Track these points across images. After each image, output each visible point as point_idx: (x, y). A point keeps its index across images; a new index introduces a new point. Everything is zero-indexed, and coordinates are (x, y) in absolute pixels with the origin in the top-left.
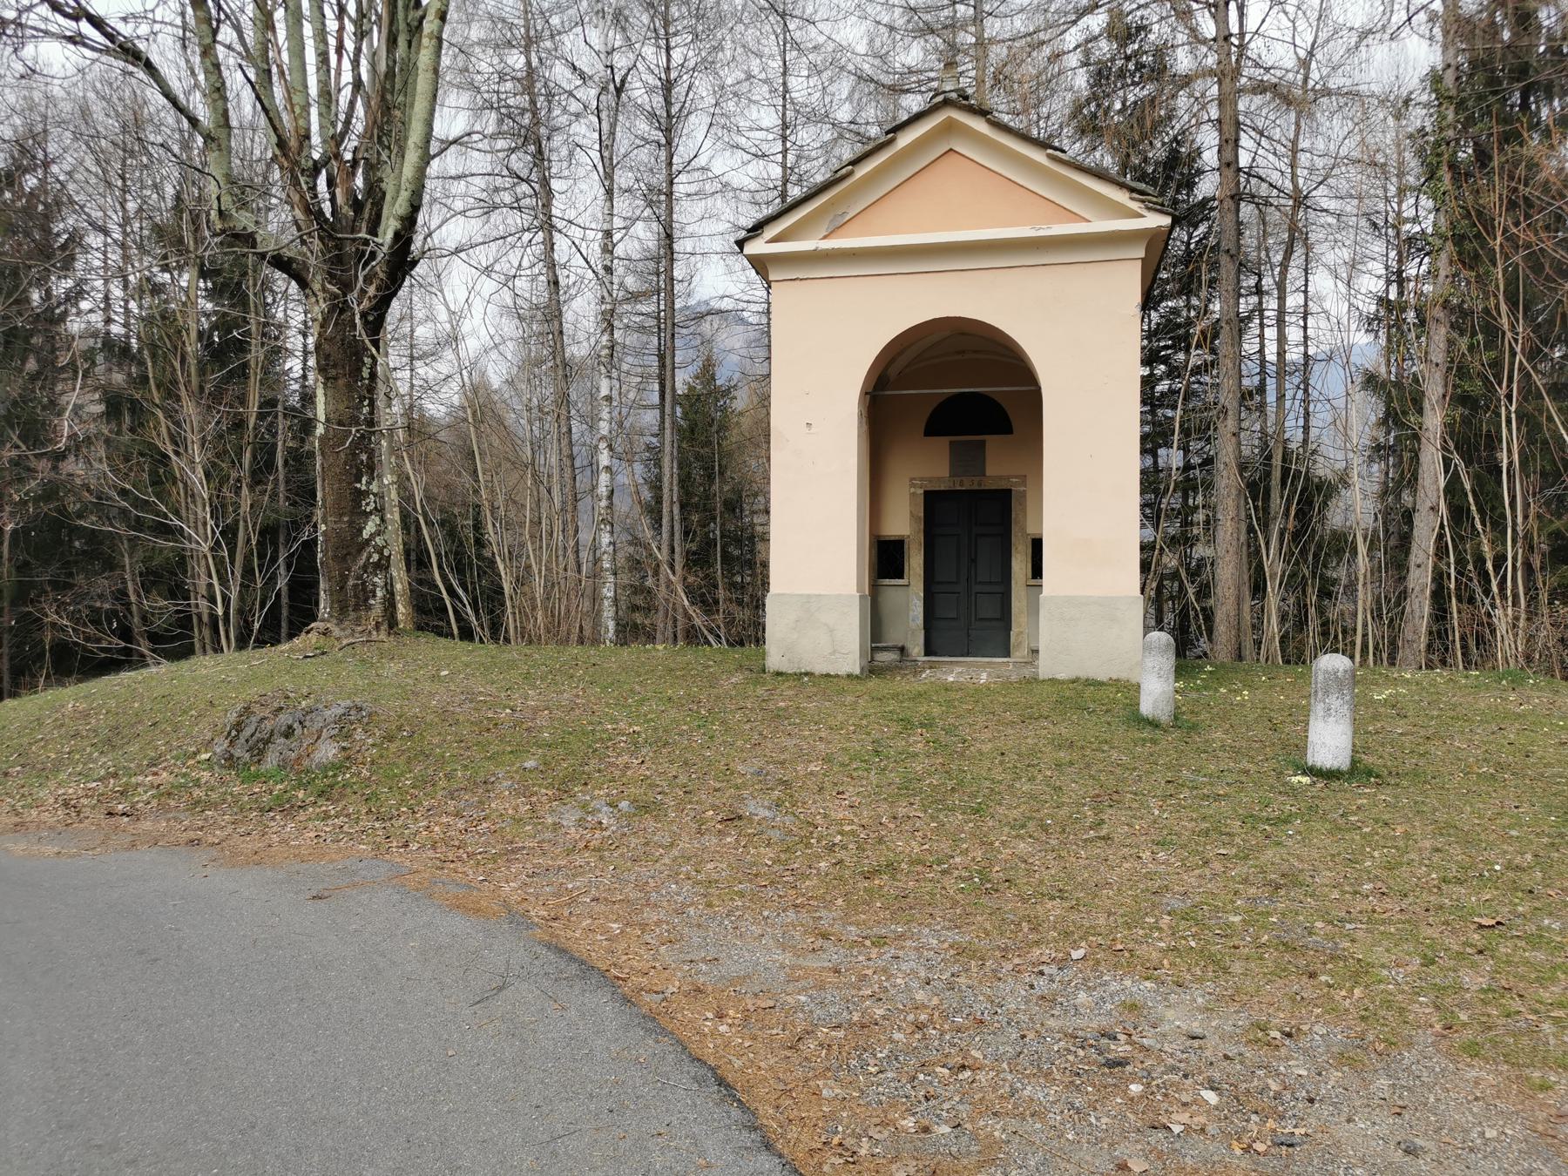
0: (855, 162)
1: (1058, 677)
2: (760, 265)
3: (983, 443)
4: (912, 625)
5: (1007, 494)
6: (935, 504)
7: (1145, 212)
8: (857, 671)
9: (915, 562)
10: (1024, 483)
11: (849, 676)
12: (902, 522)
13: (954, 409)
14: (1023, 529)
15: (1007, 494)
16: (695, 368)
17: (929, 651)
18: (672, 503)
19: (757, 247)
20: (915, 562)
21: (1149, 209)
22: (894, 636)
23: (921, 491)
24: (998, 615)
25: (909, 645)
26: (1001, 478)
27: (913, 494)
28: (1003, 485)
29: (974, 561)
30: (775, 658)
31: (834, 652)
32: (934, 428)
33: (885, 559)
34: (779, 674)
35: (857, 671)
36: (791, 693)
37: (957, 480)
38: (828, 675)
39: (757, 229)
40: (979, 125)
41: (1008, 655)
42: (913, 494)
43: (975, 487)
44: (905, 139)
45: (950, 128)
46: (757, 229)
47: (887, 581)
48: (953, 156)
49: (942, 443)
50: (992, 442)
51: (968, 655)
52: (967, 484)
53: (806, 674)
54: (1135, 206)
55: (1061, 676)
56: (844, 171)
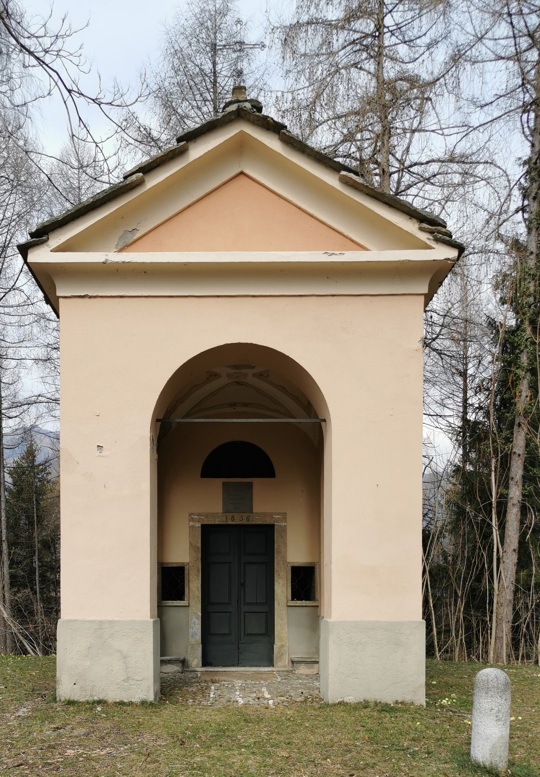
0: (147, 169)
1: (347, 700)
2: (46, 279)
3: (250, 486)
4: (192, 640)
5: (271, 527)
6: (211, 536)
7: (433, 244)
8: (151, 698)
9: (194, 586)
10: (285, 519)
11: (143, 703)
12: (183, 552)
13: (239, 441)
14: (284, 558)
15: (271, 527)
16: (21, 451)
17: (206, 662)
18: (491, 629)
19: (41, 255)
20: (194, 586)
21: (437, 240)
22: (177, 651)
23: (198, 525)
24: (263, 631)
25: (189, 658)
26: (264, 514)
27: (192, 527)
28: (268, 521)
29: (243, 585)
30: (66, 689)
31: (127, 679)
32: (210, 471)
33: (169, 583)
34: (70, 703)
35: (151, 698)
36: (81, 731)
37: (230, 515)
38: (121, 703)
39: (41, 235)
40: (273, 143)
41: (271, 663)
42: (192, 527)
43: (245, 522)
44: (198, 151)
45: (241, 147)
46: (41, 235)
47: (170, 603)
48: (243, 180)
49: (217, 483)
50: (258, 483)
51: (238, 665)
52: (238, 519)
53: (99, 702)
54: (424, 237)
55: (350, 699)
56: (134, 177)
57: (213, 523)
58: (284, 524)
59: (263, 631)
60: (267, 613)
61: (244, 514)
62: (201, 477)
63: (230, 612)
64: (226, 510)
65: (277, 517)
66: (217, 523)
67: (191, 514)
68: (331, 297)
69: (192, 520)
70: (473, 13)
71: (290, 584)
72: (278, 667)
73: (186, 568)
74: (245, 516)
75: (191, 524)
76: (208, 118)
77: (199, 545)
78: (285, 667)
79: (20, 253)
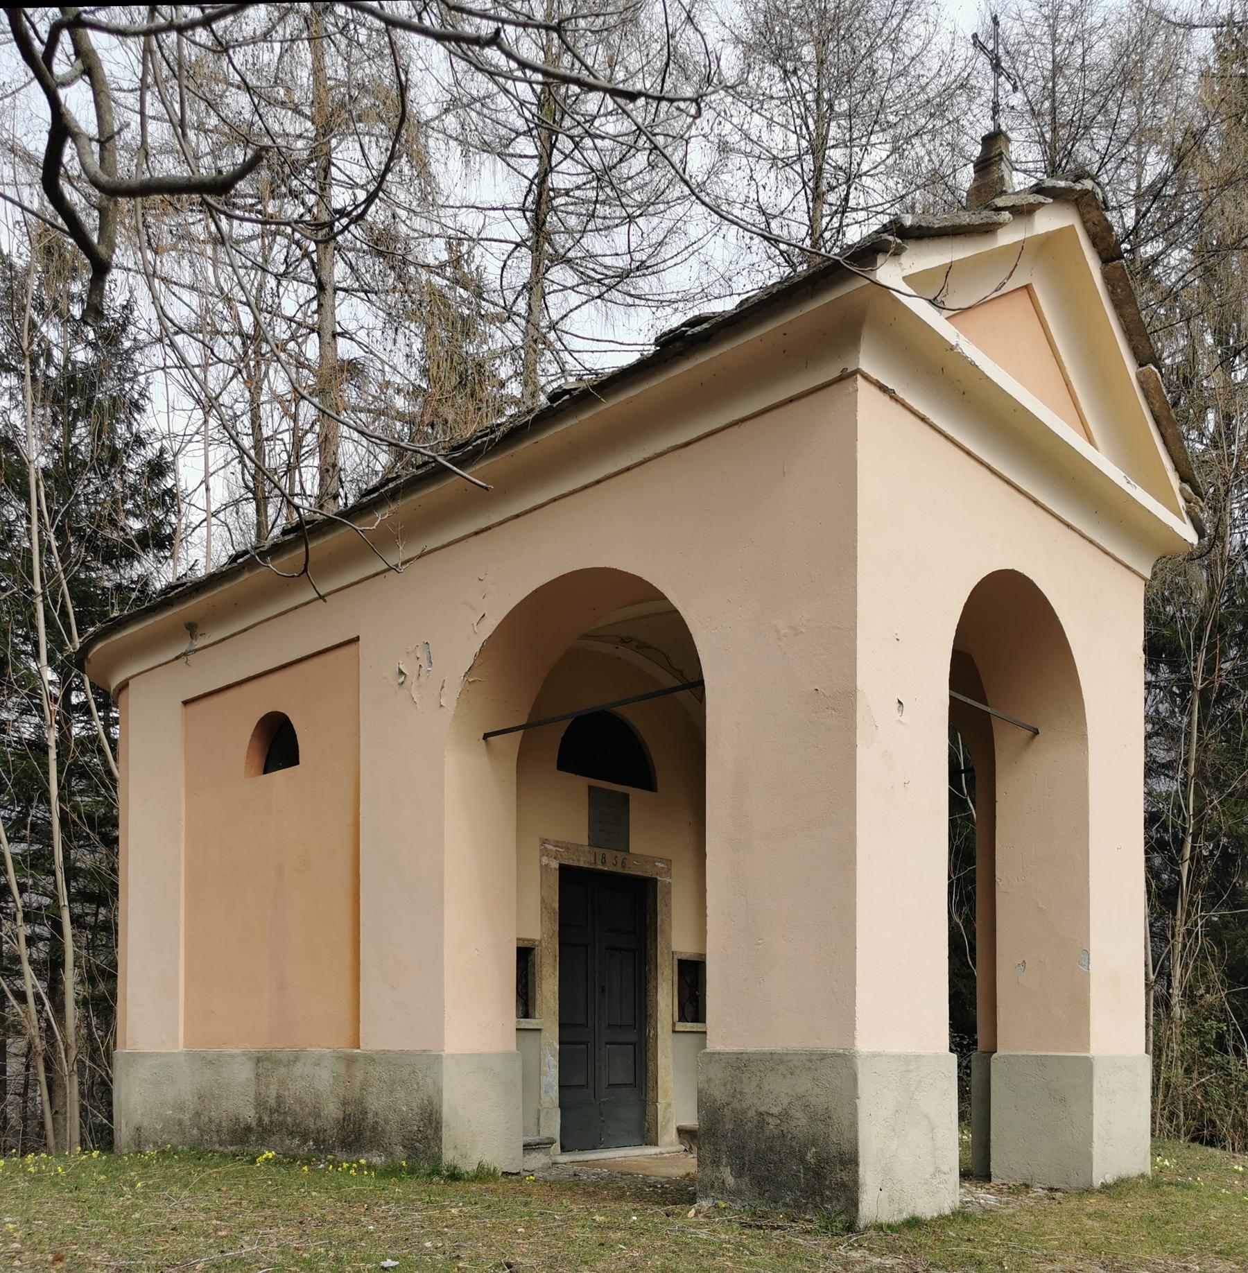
10: (668, 872)
23: (555, 865)
24: (630, 1079)
29: (603, 989)
42: (545, 868)
49: (580, 785)
57: (575, 863)
58: (668, 880)
59: (630, 1079)
60: (634, 1044)
61: (618, 854)
62: (559, 768)
63: (586, 1043)
64: (594, 842)
65: (660, 865)
66: (582, 864)
67: (544, 841)
68: (515, 521)
69: (544, 852)
70: (738, 138)
71: (676, 993)
72: (665, 1146)
73: (537, 951)
74: (610, 854)
75: (545, 860)
76: (38, 179)
77: (556, 905)
78: (672, 1145)
79: (44, 169)
